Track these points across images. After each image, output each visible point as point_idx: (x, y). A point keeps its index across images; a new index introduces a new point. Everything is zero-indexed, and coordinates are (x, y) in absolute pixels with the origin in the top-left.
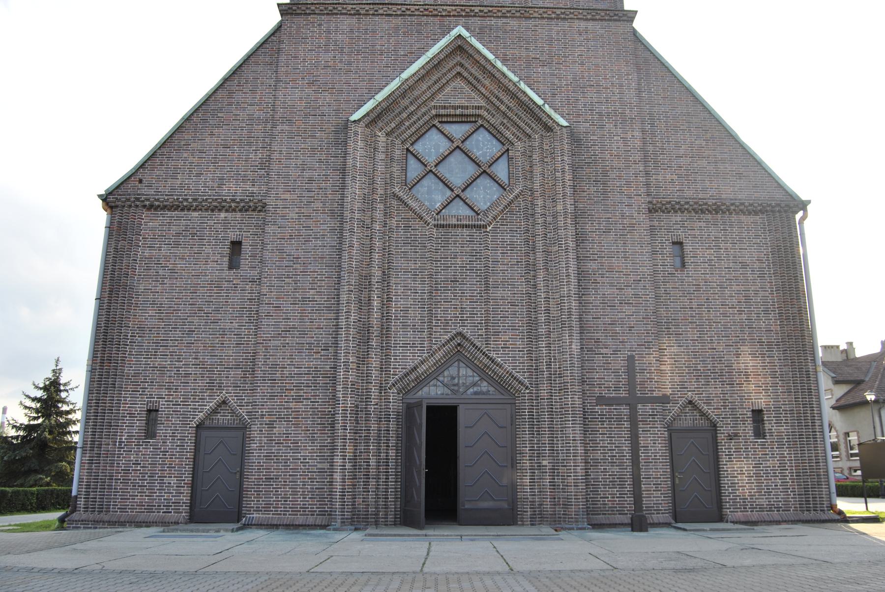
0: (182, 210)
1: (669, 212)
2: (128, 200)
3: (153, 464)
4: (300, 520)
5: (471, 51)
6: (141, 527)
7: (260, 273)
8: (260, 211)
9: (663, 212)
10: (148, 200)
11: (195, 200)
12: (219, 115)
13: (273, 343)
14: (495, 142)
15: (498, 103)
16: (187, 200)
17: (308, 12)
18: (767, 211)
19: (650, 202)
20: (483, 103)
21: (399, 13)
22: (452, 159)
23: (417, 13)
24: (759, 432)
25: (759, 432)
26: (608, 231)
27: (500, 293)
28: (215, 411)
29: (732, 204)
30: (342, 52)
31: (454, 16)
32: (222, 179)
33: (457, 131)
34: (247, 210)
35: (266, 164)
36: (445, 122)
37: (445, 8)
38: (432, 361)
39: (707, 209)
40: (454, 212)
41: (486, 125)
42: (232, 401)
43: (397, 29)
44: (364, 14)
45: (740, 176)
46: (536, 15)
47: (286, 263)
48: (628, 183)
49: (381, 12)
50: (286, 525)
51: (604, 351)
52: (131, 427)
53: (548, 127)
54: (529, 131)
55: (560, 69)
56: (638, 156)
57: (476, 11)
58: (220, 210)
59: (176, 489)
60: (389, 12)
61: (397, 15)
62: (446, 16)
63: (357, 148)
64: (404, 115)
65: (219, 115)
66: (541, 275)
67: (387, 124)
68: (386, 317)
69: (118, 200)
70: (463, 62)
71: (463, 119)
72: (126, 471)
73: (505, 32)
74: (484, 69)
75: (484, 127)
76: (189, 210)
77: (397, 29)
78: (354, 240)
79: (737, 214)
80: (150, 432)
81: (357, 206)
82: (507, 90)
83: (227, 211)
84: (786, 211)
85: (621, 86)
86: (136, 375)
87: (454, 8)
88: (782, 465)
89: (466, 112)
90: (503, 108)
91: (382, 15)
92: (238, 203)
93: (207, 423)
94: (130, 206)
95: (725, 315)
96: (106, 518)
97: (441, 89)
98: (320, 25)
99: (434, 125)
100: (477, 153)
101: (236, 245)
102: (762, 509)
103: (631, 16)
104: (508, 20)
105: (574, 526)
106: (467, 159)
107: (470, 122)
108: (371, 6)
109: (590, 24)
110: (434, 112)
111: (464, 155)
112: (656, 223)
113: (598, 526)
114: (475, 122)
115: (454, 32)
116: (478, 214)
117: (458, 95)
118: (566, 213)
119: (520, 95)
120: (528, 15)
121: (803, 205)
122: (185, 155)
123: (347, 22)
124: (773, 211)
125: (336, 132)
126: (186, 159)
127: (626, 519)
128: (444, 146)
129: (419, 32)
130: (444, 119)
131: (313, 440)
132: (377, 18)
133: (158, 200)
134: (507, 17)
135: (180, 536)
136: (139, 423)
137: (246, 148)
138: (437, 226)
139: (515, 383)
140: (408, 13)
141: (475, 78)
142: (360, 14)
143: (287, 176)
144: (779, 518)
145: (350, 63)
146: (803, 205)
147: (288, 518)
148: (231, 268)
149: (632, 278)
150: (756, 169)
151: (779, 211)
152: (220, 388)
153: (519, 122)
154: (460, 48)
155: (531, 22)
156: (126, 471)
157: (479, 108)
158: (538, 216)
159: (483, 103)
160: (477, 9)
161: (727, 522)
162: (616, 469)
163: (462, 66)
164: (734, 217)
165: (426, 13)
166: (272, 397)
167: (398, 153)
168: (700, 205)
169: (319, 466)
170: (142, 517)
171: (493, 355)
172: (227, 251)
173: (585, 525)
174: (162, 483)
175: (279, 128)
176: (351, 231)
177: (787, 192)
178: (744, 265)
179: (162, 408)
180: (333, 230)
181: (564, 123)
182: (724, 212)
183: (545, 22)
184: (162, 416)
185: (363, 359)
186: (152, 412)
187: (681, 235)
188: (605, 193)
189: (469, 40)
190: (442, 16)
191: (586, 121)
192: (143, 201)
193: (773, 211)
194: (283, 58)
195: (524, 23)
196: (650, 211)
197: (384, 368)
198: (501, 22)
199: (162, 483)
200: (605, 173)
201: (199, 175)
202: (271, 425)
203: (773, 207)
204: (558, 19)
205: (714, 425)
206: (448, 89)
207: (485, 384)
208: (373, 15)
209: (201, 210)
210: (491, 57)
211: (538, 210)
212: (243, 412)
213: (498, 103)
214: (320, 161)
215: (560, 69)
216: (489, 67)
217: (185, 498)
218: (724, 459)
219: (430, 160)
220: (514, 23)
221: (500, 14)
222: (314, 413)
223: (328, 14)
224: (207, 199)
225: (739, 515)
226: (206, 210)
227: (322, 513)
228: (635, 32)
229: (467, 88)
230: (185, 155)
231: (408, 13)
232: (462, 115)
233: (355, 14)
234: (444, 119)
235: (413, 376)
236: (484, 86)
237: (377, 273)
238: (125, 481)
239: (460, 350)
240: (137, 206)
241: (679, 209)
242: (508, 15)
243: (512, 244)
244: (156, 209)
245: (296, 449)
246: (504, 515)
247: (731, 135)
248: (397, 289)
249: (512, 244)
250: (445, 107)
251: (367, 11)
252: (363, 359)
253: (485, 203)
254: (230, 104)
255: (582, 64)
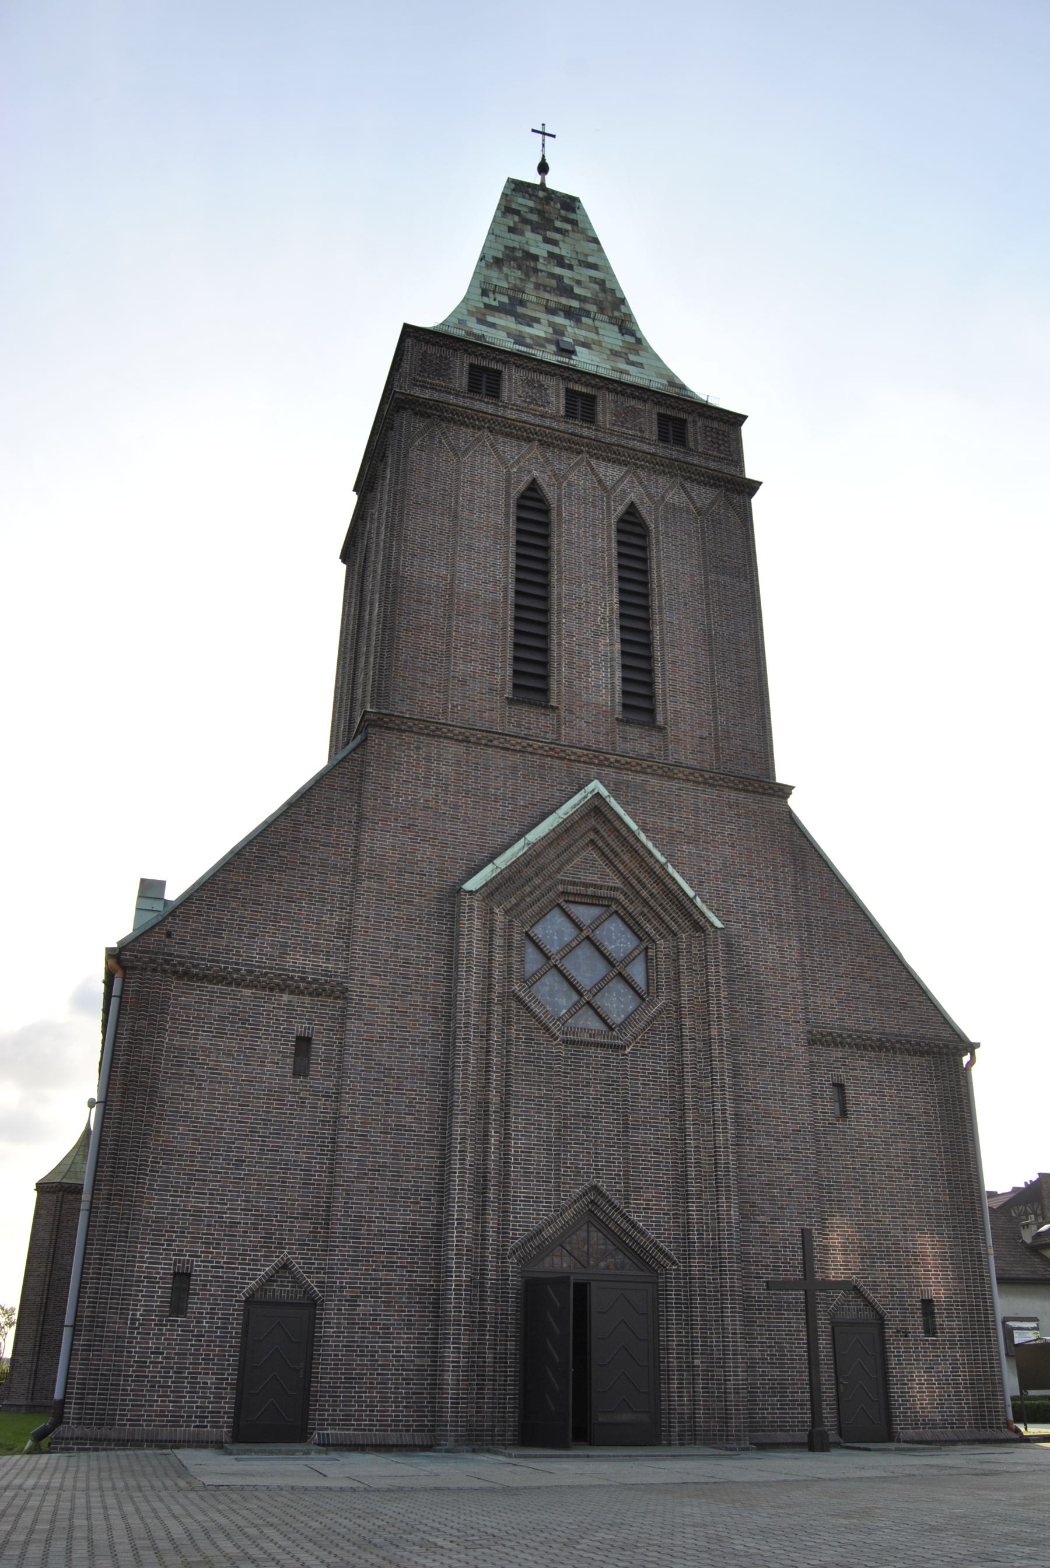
0: (229, 984)
1: (828, 1046)
2: (153, 961)
3: (182, 1355)
4: (393, 1438)
5: (610, 816)
6: (206, 1447)
7: (339, 1086)
8: (336, 998)
9: (823, 1045)
10: (181, 964)
11: (250, 972)
12: (281, 853)
13: (356, 1186)
14: (629, 935)
15: (639, 887)
16: (238, 971)
17: (403, 727)
18: (934, 1053)
19: (810, 1032)
20: (619, 884)
21: (518, 748)
22: (579, 952)
23: (540, 752)
24: (930, 1329)
25: (930, 1329)
26: (763, 1065)
27: (641, 1136)
28: (270, 1279)
29: (898, 1042)
30: (446, 791)
31: (585, 762)
32: (285, 945)
33: (585, 914)
34: (319, 995)
35: (346, 931)
36: (571, 902)
37: (574, 750)
38: (560, 1222)
39: (871, 1046)
40: (581, 1023)
41: (622, 912)
42: (297, 1265)
43: (514, 769)
44: (474, 743)
45: (904, 1006)
46: (680, 775)
47: (374, 1075)
48: (785, 1006)
49: (495, 743)
50: (376, 1445)
51: (761, 1218)
52: (149, 1298)
53: (699, 926)
54: (675, 927)
55: (708, 850)
56: (795, 973)
57: (612, 760)
58: (282, 991)
59: (213, 1389)
60: (506, 745)
61: (515, 750)
62: (575, 761)
63: (472, 925)
64: (527, 889)
65: (281, 853)
66: (690, 1117)
67: (507, 898)
68: (505, 1161)
69: (138, 959)
70: (599, 827)
71: (593, 901)
72: (142, 1364)
73: (644, 792)
74: (624, 841)
75: (619, 915)
76: (238, 985)
77: (514, 769)
78: (468, 1054)
79: (902, 1053)
80: (178, 1303)
81: (473, 1007)
82: (651, 872)
83: (292, 993)
84: (953, 1054)
85: (776, 879)
86: (159, 1220)
87: (585, 752)
88: (955, 1370)
89: (600, 892)
90: (644, 893)
91: (497, 747)
92: (309, 983)
93: (258, 1296)
94: (154, 970)
95: (890, 1178)
96: (113, 1435)
97: (570, 860)
98: (418, 748)
99: (559, 905)
100: (610, 948)
101: (303, 1043)
102: (935, 1426)
103: (786, 791)
104: (648, 778)
105: (734, 1445)
106: (596, 954)
107: (602, 906)
108: (485, 734)
109: (742, 795)
110: (560, 888)
111: (593, 949)
112: (815, 1059)
113: (762, 1447)
114: (609, 906)
115: (590, 787)
116: (612, 1029)
117: (589, 869)
118: (721, 1040)
119: (667, 881)
120: (671, 774)
121: (971, 1048)
122: (234, 905)
123: (452, 750)
124: (940, 1053)
125: (439, 900)
126: (234, 911)
127: (804, 1437)
128: (569, 932)
129: (542, 777)
130: (572, 898)
131: (409, 1326)
132: (490, 751)
133: (196, 966)
134: (646, 773)
135: (254, 1459)
136: (162, 1292)
137: (318, 905)
138: (566, 1042)
139: (660, 1257)
140: (530, 749)
141: (613, 851)
142: (469, 742)
143: (375, 954)
144: (954, 1437)
145: (456, 807)
146: (971, 1048)
147: (376, 1436)
148: (296, 1074)
149: (791, 1127)
150: (920, 999)
151: (947, 1054)
152: (281, 1246)
153: (663, 914)
154: (597, 808)
155: (675, 785)
156: (142, 1364)
157: (615, 889)
158: (686, 1039)
159: (619, 884)
160: (613, 759)
161: (899, 1442)
162: (776, 1372)
163: (597, 832)
164: (899, 1057)
165: (551, 753)
166: (355, 1262)
167: (516, 937)
168: (863, 1040)
169: (417, 1361)
170: (165, 1433)
171: (633, 1217)
172: (290, 1049)
173: (748, 1445)
174: (194, 1383)
175: (365, 884)
176: (466, 1040)
177: (954, 1030)
178: (911, 1119)
179: (196, 1271)
180: (435, 1035)
181: (718, 924)
182: (887, 1050)
183: (690, 785)
184: (196, 1280)
185: (480, 1212)
186: (182, 1279)
187: (843, 1075)
188: (759, 1015)
189: (608, 800)
190: (569, 760)
191: (738, 921)
192: (174, 965)
193: (940, 1053)
194: (369, 787)
195: (666, 783)
196: (809, 1043)
197: (503, 1230)
198: (640, 778)
199: (194, 1383)
200: (759, 990)
201: (252, 936)
202: (353, 1301)
203: (940, 1048)
204: (705, 784)
205: (881, 1318)
206: (577, 860)
207: (621, 1256)
208: (486, 745)
209: (256, 987)
210: (634, 827)
211: (686, 1032)
212: (311, 1281)
213: (639, 887)
214: (419, 938)
215: (708, 850)
216: (631, 840)
217: (227, 1406)
218: (893, 1362)
219: (554, 950)
220: (654, 781)
221: (639, 768)
222: (411, 1288)
223: (428, 735)
224: (266, 973)
225: (911, 1433)
226: (263, 988)
227: (421, 1429)
228: (790, 812)
229: (600, 862)
230: (234, 905)
231: (530, 749)
232: (593, 896)
233: (462, 741)
234: (572, 898)
235: (536, 1242)
236: (623, 862)
237: (494, 1099)
238: (139, 1379)
239: (595, 1211)
240: (164, 971)
241: (841, 1043)
242: (649, 770)
243: (655, 1072)
244: (190, 979)
245: (387, 1337)
246: (646, 1433)
247: (895, 955)
248: (517, 1122)
249: (655, 1072)
250: (574, 884)
251: (479, 739)
252: (480, 1212)
253: (619, 1015)
254: (296, 840)
255: (733, 846)
